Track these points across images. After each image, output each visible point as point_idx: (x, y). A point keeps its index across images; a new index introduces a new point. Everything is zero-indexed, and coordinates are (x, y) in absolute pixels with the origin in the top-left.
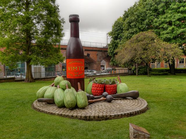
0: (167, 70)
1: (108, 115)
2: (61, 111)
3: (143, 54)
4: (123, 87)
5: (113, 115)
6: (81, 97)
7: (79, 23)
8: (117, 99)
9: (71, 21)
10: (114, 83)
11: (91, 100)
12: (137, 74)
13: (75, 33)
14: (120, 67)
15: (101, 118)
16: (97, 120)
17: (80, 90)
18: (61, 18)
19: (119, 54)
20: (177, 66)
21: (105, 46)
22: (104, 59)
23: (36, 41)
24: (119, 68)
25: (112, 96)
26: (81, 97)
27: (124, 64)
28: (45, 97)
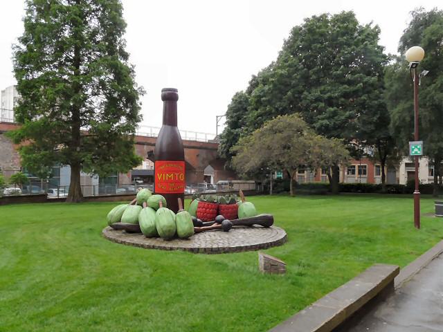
0: (325, 186)
2: (148, 242)
3: (282, 155)
6: (184, 219)
7: (178, 102)
9: (165, 98)
10: (233, 201)
11: (199, 226)
12: (271, 193)
13: (170, 117)
14: (240, 179)
17: (181, 209)
18: (139, 86)
19: (239, 155)
20: (344, 178)
21: (212, 138)
22: (211, 163)
23: (90, 127)
24: (239, 181)
26: (184, 219)
27: (248, 173)
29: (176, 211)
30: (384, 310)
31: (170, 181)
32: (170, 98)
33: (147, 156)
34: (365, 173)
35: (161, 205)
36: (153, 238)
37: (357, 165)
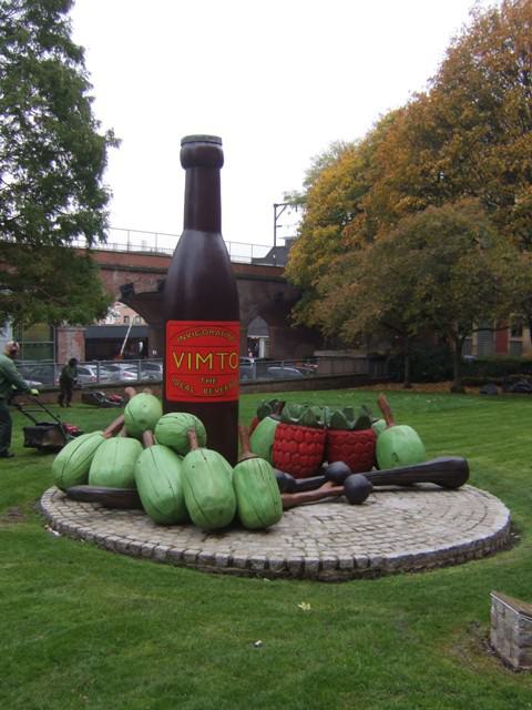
1: (375, 559)
4: (401, 439)
5: (394, 559)
7: (224, 172)
8: (382, 491)
10: (365, 423)
13: (203, 208)
15: (349, 569)
16: (274, 577)
24: (330, 353)
25: (367, 477)
28: (92, 480)
29: (233, 461)
31: (204, 372)
32: (203, 161)
33: (119, 296)
35: (194, 442)
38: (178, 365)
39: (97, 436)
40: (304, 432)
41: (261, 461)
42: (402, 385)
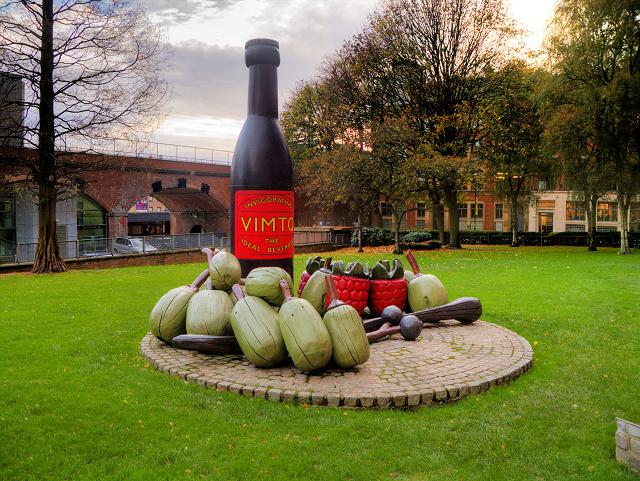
9: (251, 60)
10: (400, 273)
30: (317, 363)
33: (151, 191)
34: (480, 215)
36: (276, 372)
37: (469, 203)
38: (246, 228)
39: (182, 291)
40: (354, 282)
41: (350, 307)
42: (391, 248)
